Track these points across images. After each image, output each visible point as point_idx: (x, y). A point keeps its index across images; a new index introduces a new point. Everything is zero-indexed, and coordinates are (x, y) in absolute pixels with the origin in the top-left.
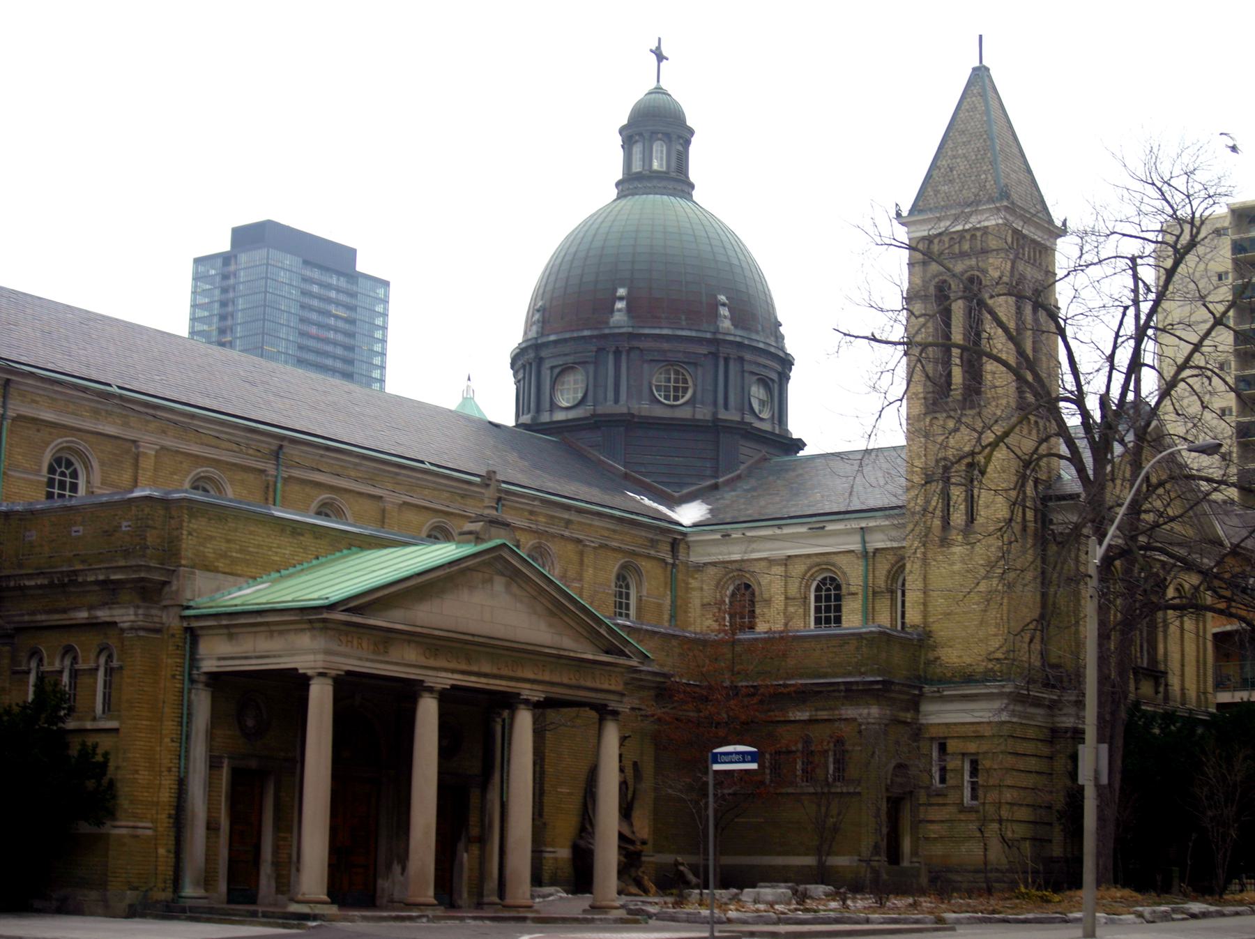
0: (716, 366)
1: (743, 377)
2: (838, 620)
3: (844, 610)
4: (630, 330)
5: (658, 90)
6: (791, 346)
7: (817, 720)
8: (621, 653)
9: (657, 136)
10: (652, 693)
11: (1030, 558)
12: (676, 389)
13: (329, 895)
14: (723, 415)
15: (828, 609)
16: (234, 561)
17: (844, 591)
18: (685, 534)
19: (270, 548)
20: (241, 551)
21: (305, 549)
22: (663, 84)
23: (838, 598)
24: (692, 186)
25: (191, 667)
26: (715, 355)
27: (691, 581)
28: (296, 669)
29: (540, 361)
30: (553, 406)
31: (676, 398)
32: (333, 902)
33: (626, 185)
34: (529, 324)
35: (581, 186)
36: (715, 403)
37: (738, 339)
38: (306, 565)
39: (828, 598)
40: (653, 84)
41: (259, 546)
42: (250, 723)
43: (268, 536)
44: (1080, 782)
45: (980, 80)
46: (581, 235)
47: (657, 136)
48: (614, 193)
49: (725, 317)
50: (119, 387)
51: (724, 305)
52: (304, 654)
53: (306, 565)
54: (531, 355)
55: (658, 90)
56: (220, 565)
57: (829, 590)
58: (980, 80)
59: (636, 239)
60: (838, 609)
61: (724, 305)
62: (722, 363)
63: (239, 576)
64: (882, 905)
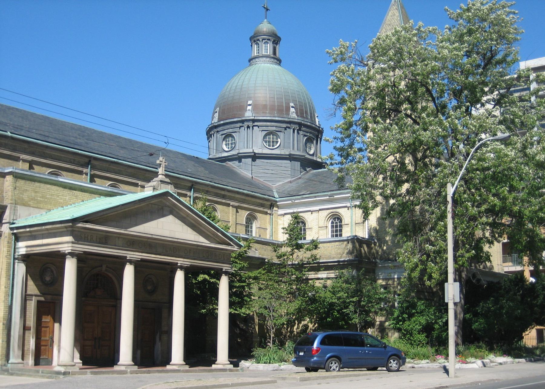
2: (341, 235)
3: (343, 231)
4: (253, 118)
7: (462, 369)
8: (229, 244)
12: (273, 142)
13: (184, 361)
15: (336, 231)
16: (39, 202)
17: (343, 223)
18: (276, 202)
19: (58, 196)
20: (42, 197)
21: (76, 196)
23: (341, 226)
25: (15, 252)
27: (279, 221)
28: (60, 251)
31: (273, 146)
32: (135, 365)
37: (299, 121)
38: (77, 204)
39: (336, 226)
41: (52, 195)
42: (48, 279)
43: (58, 191)
44: (446, 301)
50: (11, 133)
52: (64, 244)
53: (77, 204)
56: (31, 203)
57: (336, 223)
58: (448, 375)
60: (341, 231)
63: (42, 209)
64: (236, 365)
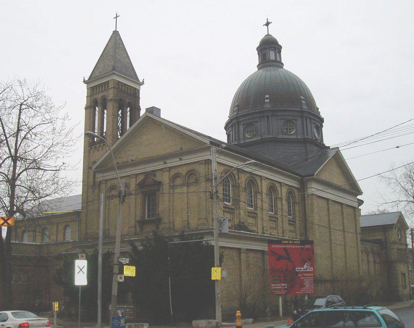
0: (303, 120)
1: (311, 125)
5: (268, 35)
6: (322, 115)
9: (269, 49)
10: (287, 232)
11: (328, 278)
14: (306, 137)
22: (270, 33)
24: (283, 64)
26: (302, 117)
29: (238, 123)
30: (244, 138)
33: (261, 65)
34: (232, 111)
35: (247, 66)
36: (304, 133)
40: (267, 34)
45: (115, 44)
46: (249, 82)
47: (269, 49)
48: (256, 69)
49: (304, 104)
51: (303, 100)
54: (235, 121)
55: (268, 35)
58: (115, 44)
59: (265, 82)
61: (303, 100)
62: (304, 119)
